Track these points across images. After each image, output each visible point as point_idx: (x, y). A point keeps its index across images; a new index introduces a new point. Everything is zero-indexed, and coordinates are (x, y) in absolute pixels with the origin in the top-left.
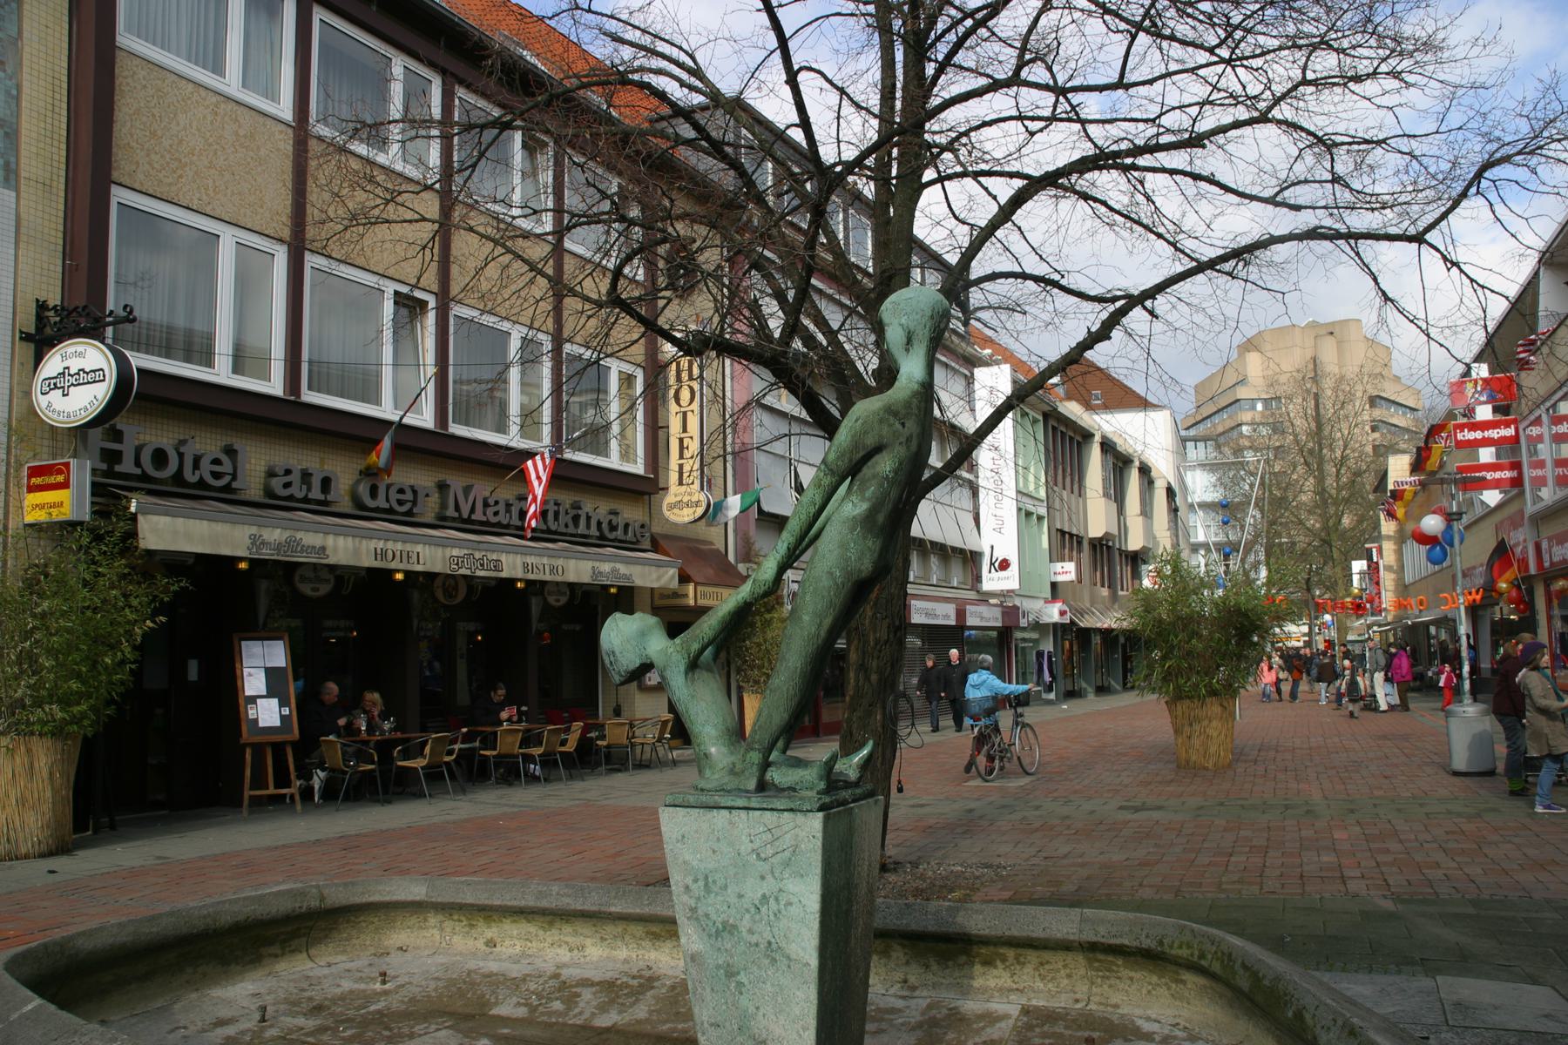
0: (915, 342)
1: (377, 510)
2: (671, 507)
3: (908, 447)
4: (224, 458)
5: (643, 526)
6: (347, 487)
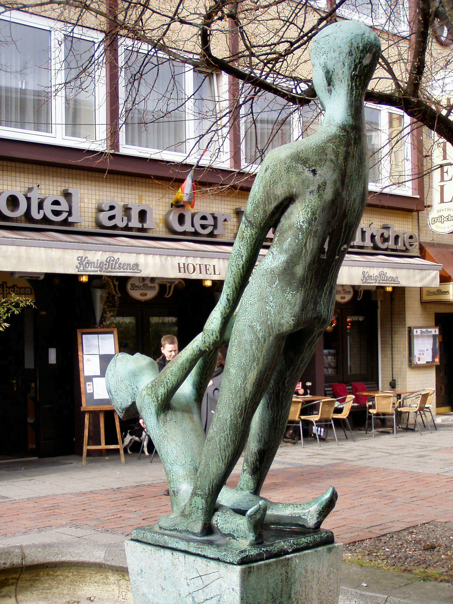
0: (336, 82)
1: (184, 233)
2: (435, 220)
3: (320, 196)
4: (62, 200)
5: (411, 237)
6: (161, 217)
